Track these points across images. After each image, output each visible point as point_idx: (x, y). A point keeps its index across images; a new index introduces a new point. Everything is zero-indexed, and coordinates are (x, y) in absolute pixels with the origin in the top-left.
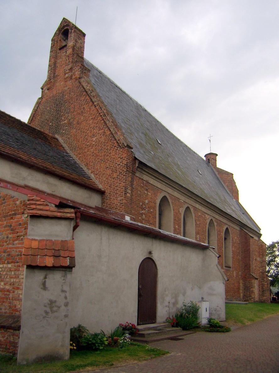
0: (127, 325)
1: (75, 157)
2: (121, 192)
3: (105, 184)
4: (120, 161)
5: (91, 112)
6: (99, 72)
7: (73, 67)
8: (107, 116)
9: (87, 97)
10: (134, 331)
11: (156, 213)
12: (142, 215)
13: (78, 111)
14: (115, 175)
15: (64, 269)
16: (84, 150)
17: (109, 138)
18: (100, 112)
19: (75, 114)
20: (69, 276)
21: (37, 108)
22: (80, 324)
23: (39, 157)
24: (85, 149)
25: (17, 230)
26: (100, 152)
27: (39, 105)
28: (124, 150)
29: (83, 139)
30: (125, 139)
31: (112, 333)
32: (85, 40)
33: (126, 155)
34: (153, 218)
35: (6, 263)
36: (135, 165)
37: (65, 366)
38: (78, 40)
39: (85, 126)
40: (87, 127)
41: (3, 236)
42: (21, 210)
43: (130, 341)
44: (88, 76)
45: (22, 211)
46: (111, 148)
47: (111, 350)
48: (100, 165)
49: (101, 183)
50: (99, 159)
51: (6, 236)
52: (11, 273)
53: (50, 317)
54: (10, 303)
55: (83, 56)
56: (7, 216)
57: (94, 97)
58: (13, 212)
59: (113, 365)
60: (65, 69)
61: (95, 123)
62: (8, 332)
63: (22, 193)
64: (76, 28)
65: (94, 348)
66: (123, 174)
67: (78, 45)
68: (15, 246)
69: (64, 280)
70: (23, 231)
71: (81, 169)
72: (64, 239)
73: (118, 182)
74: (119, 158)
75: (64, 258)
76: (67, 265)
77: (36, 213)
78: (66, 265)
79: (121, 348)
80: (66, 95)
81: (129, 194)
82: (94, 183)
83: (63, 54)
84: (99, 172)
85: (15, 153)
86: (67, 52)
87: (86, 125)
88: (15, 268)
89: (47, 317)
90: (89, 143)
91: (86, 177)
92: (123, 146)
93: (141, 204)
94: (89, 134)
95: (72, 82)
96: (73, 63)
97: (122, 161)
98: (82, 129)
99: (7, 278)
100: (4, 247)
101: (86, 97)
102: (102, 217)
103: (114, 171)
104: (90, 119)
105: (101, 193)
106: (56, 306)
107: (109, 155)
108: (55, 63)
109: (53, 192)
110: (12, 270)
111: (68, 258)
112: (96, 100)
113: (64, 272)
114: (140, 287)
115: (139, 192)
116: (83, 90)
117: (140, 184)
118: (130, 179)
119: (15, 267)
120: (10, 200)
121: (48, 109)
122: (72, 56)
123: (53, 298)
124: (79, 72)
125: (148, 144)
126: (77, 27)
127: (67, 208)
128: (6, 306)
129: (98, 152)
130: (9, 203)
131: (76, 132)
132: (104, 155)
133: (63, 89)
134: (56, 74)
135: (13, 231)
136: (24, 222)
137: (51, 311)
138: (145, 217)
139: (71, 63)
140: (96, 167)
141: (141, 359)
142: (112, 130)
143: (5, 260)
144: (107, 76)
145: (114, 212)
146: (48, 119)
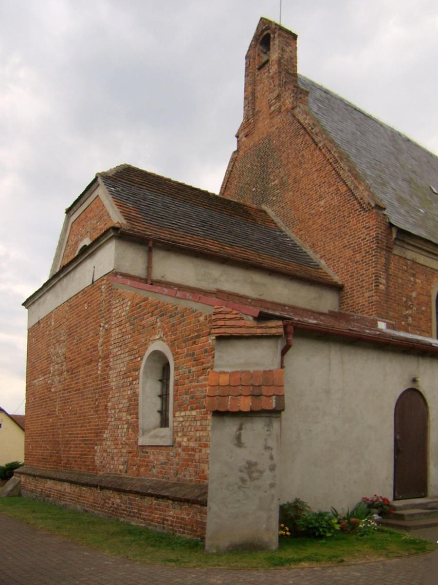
0: (375, 499)
1: (294, 236)
2: (369, 283)
3: (343, 273)
4: (366, 233)
5: (315, 160)
6: (323, 91)
7: (281, 93)
8: (339, 161)
9: (307, 137)
10: (387, 509)
11: (431, 312)
12: (407, 318)
13: (294, 162)
14: (358, 257)
15: (267, 415)
16: (307, 223)
17: (345, 197)
18: (328, 157)
19: (290, 166)
20: (276, 425)
21: (232, 168)
22: (298, 498)
23: (237, 245)
24: (309, 222)
25: (202, 360)
26: (332, 222)
27: (234, 163)
28: (370, 214)
29: (304, 205)
30: (372, 195)
31: (350, 512)
32: (298, 44)
33: (374, 221)
34: (426, 321)
35: (189, 408)
36: (392, 236)
37: (269, 560)
38: (285, 48)
39: (306, 184)
40: (310, 186)
41: (183, 370)
42: (207, 329)
43: (376, 525)
44: (306, 103)
45: (208, 330)
46: (350, 213)
47: (343, 539)
48: (334, 243)
49: (337, 273)
50: (332, 235)
51: (187, 369)
52: (197, 424)
53: (248, 487)
54: (196, 467)
55: (296, 71)
56: (188, 340)
57: (317, 135)
58: (196, 334)
59: (342, 561)
60: (269, 98)
61: (321, 177)
62: (194, 507)
63: (206, 304)
64: (281, 29)
65: (317, 534)
66: (370, 254)
67: (286, 56)
68: (200, 383)
69: (268, 430)
70: (210, 360)
71: (304, 254)
72: (267, 369)
73: (364, 268)
74: (364, 229)
75: (267, 397)
76: (271, 408)
77: (225, 333)
78: (269, 409)
79: (362, 536)
80: (274, 140)
81: (384, 285)
82: (325, 274)
83: (264, 75)
84: (332, 255)
85: (200, 243)
86: (271, 71)
87: (308, 182)
88: (201, 415)
89: (244, 487)
90: (314, 210)
91: (313, 266)
92: (369, 208)
93: (404, 299)
94: (313, 196)
95: (281, 117)
96: (281, 87)
97: (368, 232)
98: (302, 189)
99: (190, 431)
100: (185, 386)
101: (305, 137)
102: (328, 329)
103: (356, 251)
104: (314, 171)
105: (338, 288)
106: (258, 471)
107: (346, 226)
108: (253, 93)
109: (260, 295)
110: (197, 419)
111: (274, 397)
112: (320, 138)
113: (267, 419)
114: (398, 437)
115: (400, 281)
116: (300, 127)
117: (401, 267)
118: (383, 260)
119: (202, 414)
120: (191, 315)
121: (249, 166)
122: (278, 77)
123: (253, 459)
124: (291, 98)
125: (415, 197)
126: (283, 28)
127: (272, 321)
128: (190, 471)
129: (330, 223)
130: (189, 321)
131: (293, 196)
132: (339, 227)
133: (268, 132)
134: (256, 110)
135: (197, 361)
136: (211, 347)
137: (250, 477)
138: (412, 320)
139: (278, 87)
140: (327, 247)
141: (392, 556)
142: (349, 183)
143: (188, 406)
144: (337, 95)
145: (359, 318)
146: (249, 182)
